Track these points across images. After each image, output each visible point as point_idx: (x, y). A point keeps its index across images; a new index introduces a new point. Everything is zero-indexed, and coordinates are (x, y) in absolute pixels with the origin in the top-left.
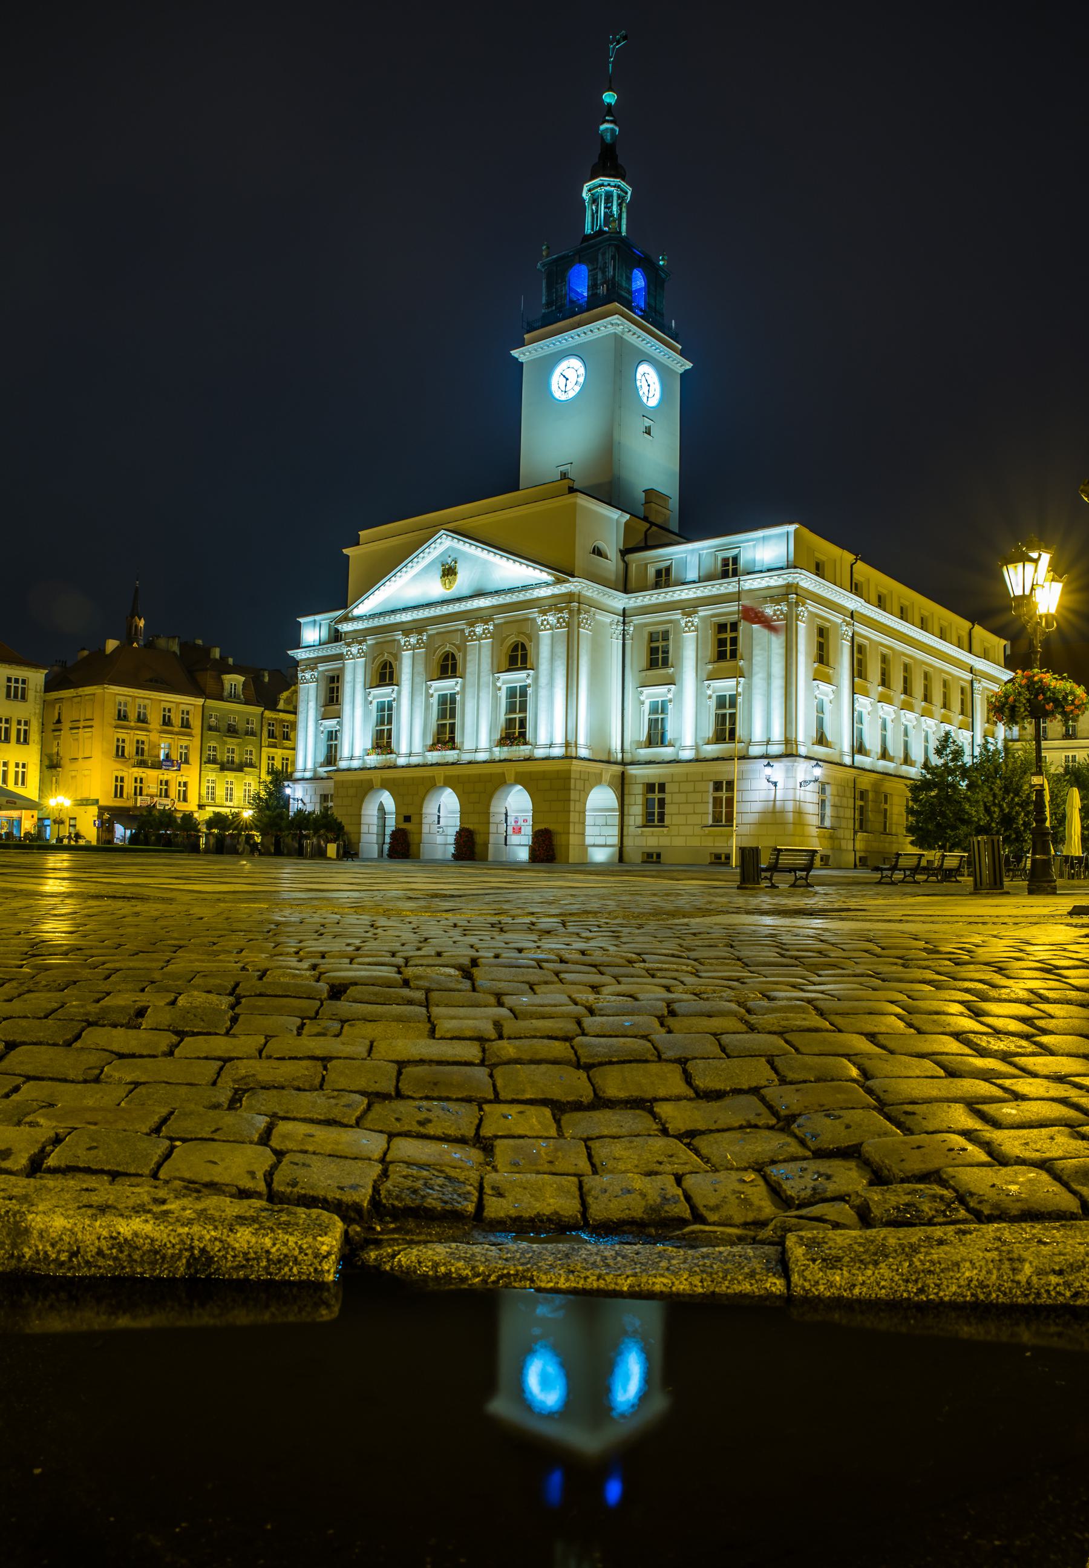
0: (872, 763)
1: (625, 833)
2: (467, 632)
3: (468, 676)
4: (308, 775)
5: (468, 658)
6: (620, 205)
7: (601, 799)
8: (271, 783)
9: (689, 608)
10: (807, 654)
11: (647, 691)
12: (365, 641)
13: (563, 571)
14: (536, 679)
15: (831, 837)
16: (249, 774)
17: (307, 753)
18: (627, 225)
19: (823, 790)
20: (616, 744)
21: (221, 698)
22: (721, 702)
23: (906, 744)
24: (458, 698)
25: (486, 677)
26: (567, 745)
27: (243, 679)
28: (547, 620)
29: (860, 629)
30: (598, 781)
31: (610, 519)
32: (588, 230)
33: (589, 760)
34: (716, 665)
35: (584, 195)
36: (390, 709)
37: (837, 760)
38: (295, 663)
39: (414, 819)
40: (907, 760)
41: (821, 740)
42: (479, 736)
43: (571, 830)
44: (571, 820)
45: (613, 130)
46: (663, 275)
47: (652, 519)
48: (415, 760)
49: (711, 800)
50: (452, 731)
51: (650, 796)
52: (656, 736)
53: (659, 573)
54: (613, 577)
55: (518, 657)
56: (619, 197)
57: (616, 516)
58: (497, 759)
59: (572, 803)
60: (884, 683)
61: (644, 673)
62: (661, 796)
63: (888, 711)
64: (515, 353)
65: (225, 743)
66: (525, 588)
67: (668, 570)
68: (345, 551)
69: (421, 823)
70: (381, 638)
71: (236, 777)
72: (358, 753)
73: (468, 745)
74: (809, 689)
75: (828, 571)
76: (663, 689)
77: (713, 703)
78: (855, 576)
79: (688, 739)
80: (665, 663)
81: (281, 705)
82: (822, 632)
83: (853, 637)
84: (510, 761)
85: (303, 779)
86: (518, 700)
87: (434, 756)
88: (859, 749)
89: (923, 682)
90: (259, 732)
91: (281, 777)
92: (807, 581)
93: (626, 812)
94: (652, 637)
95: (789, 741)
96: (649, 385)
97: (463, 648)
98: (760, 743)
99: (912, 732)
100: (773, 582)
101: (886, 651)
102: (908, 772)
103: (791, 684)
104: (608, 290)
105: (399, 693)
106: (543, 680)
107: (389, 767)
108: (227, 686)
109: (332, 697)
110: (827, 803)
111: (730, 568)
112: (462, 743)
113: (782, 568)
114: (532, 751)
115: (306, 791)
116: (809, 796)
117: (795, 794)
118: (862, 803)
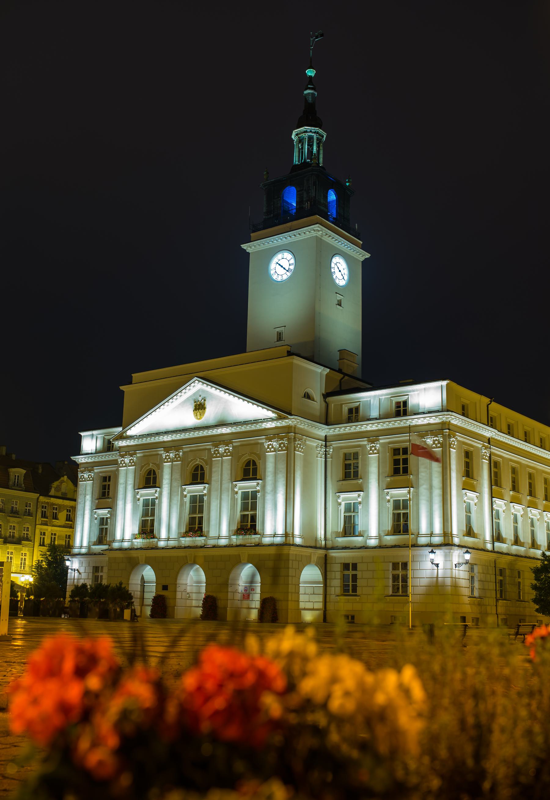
0: (508, 548)
1: (328, 600)
2: (212, 450)
3: (213, 483)
4: (84, 551)
5: (213, 470)
6: (318, 147)
7: (310, 574)
8: (50, 555)
9: (373, 437)
10: (458, 471)
11: (343, 496)
12: (135, 454)
13: (283, 411)
14: (264, 487)
15: (479, 604)
16: (25, 546)
17: (83, 535)
18: (323, 158)
19: (472, 570)
20: (320, 533)
21: (7, 487)
22: (397, 504)
23: (533, 532)
24: (205, 498)
25: (227, 484)
26: (286, 535)
27: (24, 471)
28: (272, 445)
29: (495, 450)
30: (308, 561)
31: (316, 372)
32: (296, 160)
33: (302, 546)
34: (393, 478)
35: (293, 137)
36: (153, 504)
37: (481, 546)
38: (76, 465)
39: (169, 588)
40: (534, 545)
41: (470, 532)
42: (221, 527)
43: (290, 598)
44: (290, 591)
45: (313, 94)
46: (349, 193)
47: (345, 371)
48: (172, 543)
49: (391, 577)
50: (201, 523)
51: (346, 572)
52: (349, 528)
53: (350, 411)
54: (318, 413)
55: (250, 470)
56: (318, 139)
57: (319, 370)
58: (234, 544)
59: (290, 578)
60: (514, 488)
61: (341, 483)
62: (354, 572)
63: (518, 509)
64: (244, 246)
65: (8, 521)
66: (256, 421)
67: (357, 409)
68: (122, 388)
69: (175, 591)
70: (148, 452)
71: (15, 549)
72: (128, 536)
73: (213, 533)
74: (459, 496)
75: (471, 411)
76: (354, 495)
77: (390, 506)
78: (490, 412)
79: (373, 531)
80: (356, 475)
81: (52, 492)
82: (467, 454)
83: (490, 457)
84: (245, 546)
85: (79, 554)
86: (250, 502)
87: (186, 541)
88: (498, 537)
89: (543, 486)
90: (34, 513)
91: (58, 553)
92: (456, 420)
93: (328, 585)
94: (346, 457)
95: (447, 534)
96: (340, 271)
97: (209, 462)
98: (426, 535)
99: (537, 524)
100: (432, 421)
101: (514, 465)
102: (535, 553)
103: (447, 493)
104: (311, 205)
105: (161, 493)
106: (269, 488)
107: (152, 548)
108: (12, 477)
109: (106, 493)
110: (476, 579)
111: (402, 409)
112: (208, 532)
113: (438, 411)
114: (260, 539)
115: (81, 563)
116: (462, 573)
117: (452, 573)
118: (501, 578)
